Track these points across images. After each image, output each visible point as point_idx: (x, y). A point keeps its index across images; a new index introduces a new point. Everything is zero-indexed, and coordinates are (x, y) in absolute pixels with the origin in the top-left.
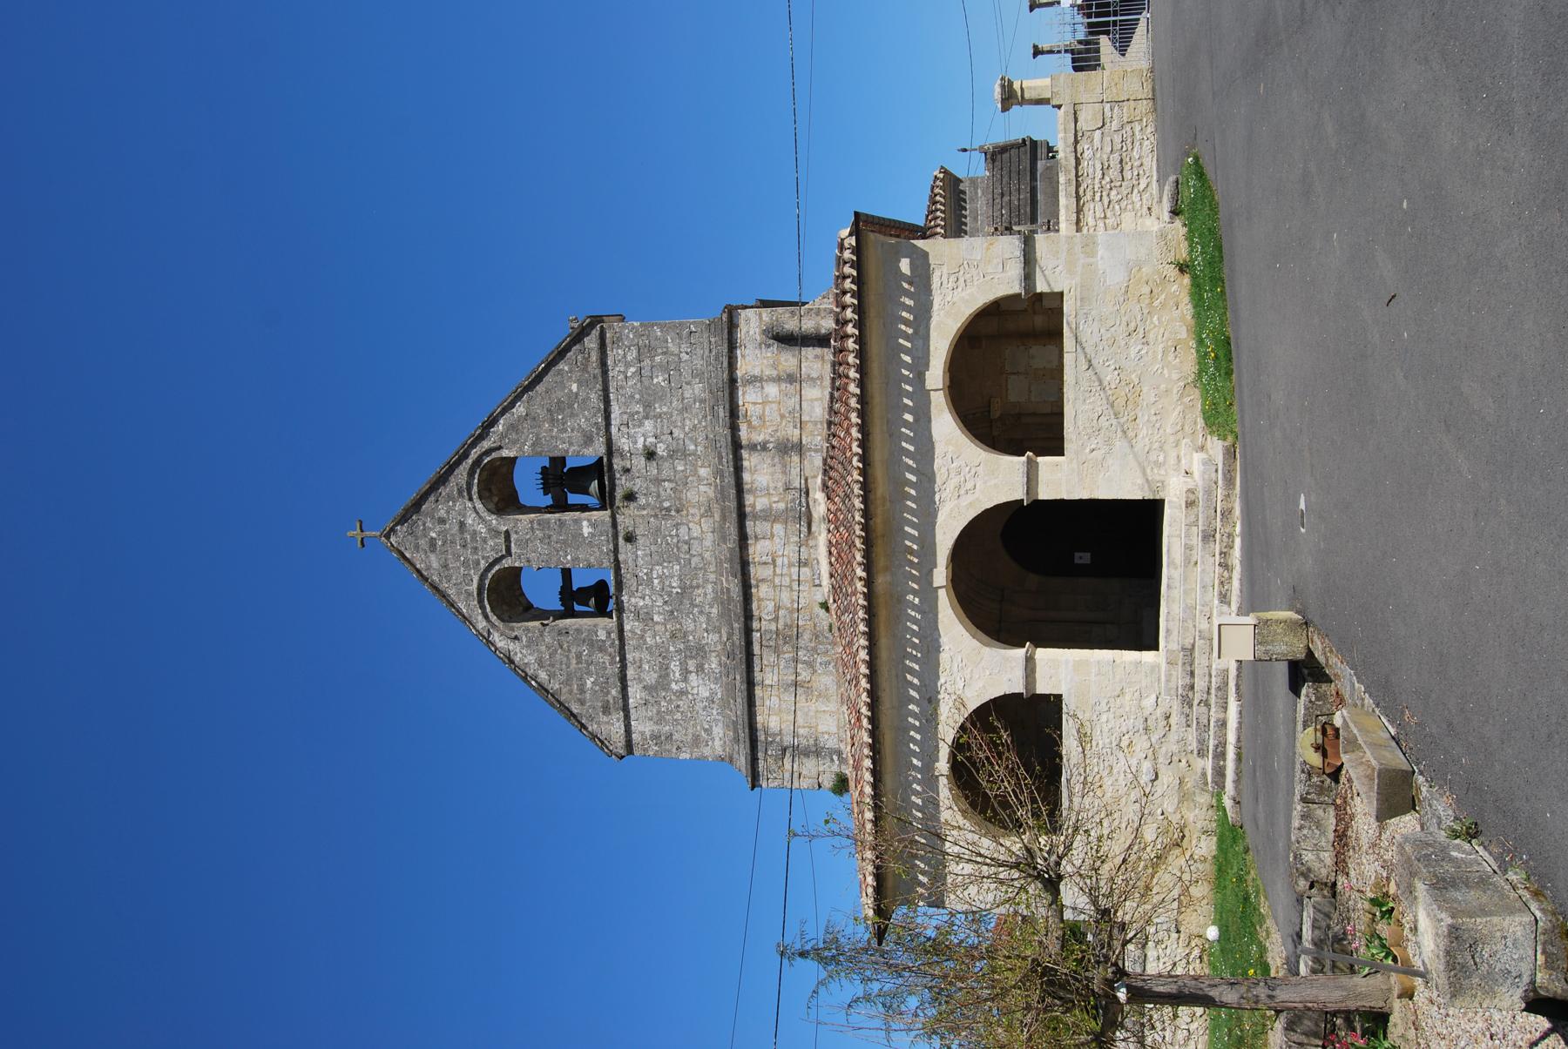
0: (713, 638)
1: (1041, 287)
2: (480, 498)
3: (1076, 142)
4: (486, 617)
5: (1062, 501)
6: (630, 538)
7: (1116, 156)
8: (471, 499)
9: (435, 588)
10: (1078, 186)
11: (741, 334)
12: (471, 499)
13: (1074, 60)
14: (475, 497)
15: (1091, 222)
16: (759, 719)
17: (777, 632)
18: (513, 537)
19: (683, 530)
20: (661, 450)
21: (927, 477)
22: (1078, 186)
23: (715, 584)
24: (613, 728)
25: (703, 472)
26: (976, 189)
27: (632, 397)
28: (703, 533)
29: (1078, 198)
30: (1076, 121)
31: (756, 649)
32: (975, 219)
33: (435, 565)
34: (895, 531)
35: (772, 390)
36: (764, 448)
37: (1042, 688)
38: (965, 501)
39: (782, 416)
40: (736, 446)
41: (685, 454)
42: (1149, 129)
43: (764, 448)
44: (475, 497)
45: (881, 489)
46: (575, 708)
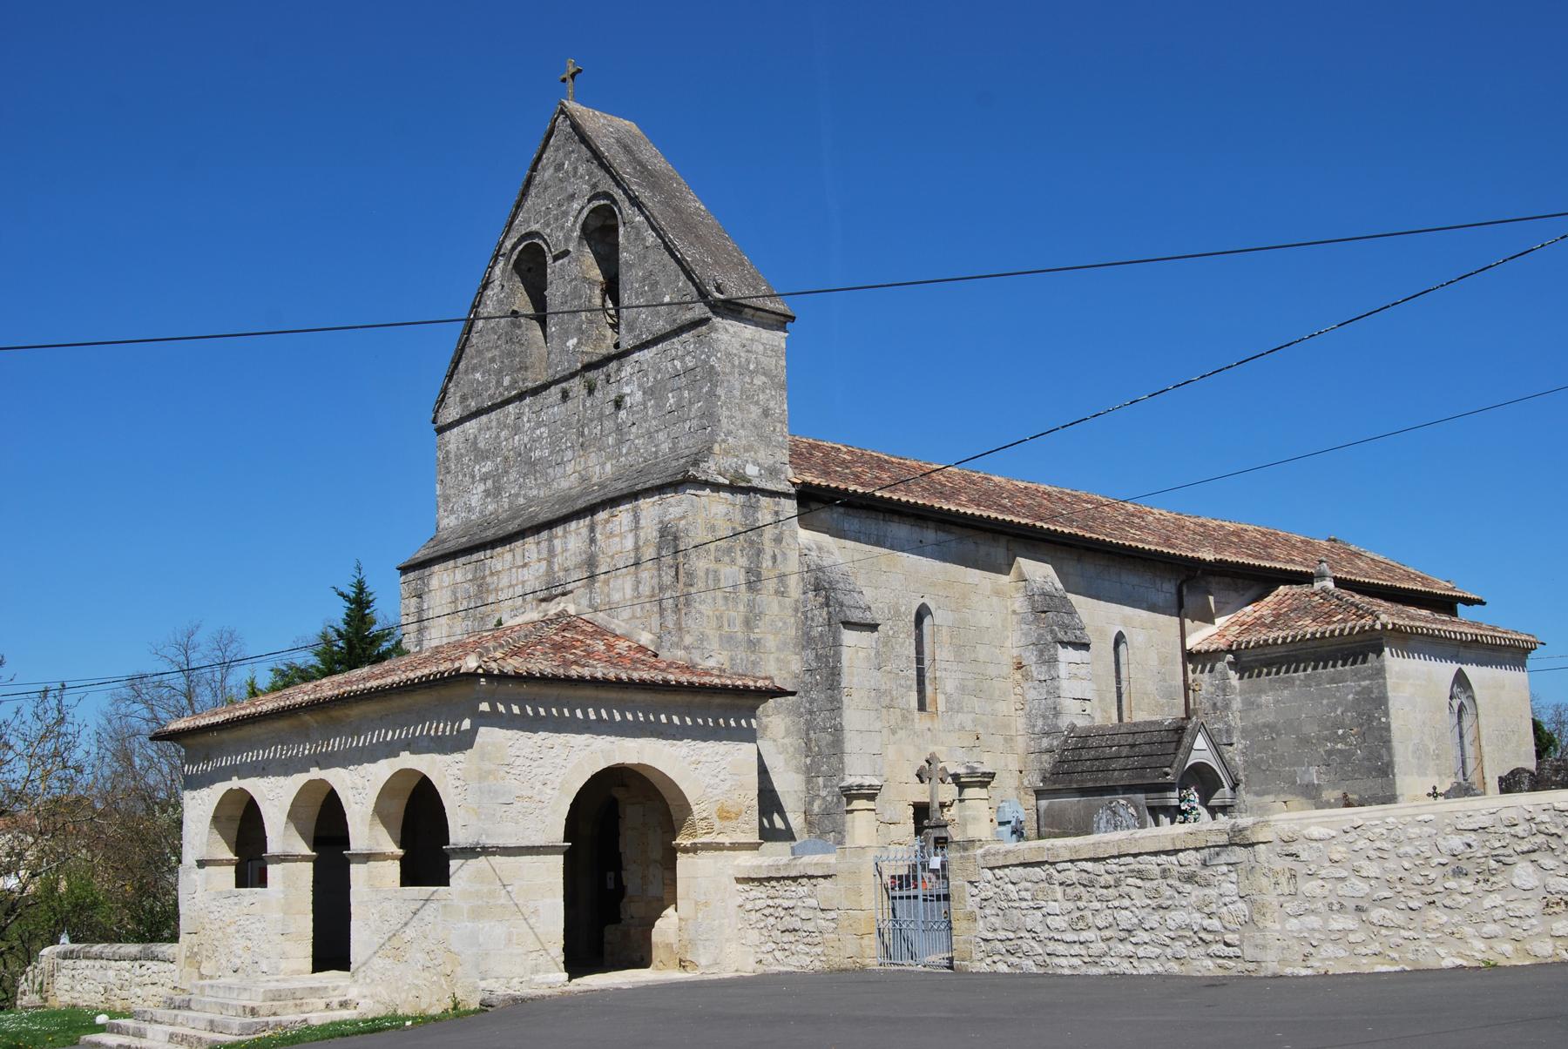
0: (505, 503)
1: (454, 864)
2: (592, 211)
3: (810, 877)
4: (514, 247)
5: (349, 887)
6: (565, 396)
7: (798, 925)
8: (589, 201)
9: (529, 182)
10: (778, 879)
11: (671, 498)
12: (589, 201)
13: (900, 877)
14: (591, 206)
15: (753, 894)
16: (436, 568)
17: (484, 578)
18: (566, 260)
19: (569, 454)
20: (623, 414)
21: (560, 726)
22: (778, 879)
23: (533, 494)
24: (451, 413)
25: (608, 466)
26: (1369, 677)
27: (659, 371)
28: (574, 474)
29: (769, 879)
30: (825, 877)
31: (475, 557)
32: (1332, 680)
33: (547, 175)
34: (336, 728)
35: (629, 543)
36: (592, 541)
37: (273, 871)
38: (451, 782)
39: (612, 557)
40: (592, 510)
41: (620, 443)
42: (817, 963)
43: (592, 541)
44: (596, 203)
45: (356, 711)
46: (462, 366)
